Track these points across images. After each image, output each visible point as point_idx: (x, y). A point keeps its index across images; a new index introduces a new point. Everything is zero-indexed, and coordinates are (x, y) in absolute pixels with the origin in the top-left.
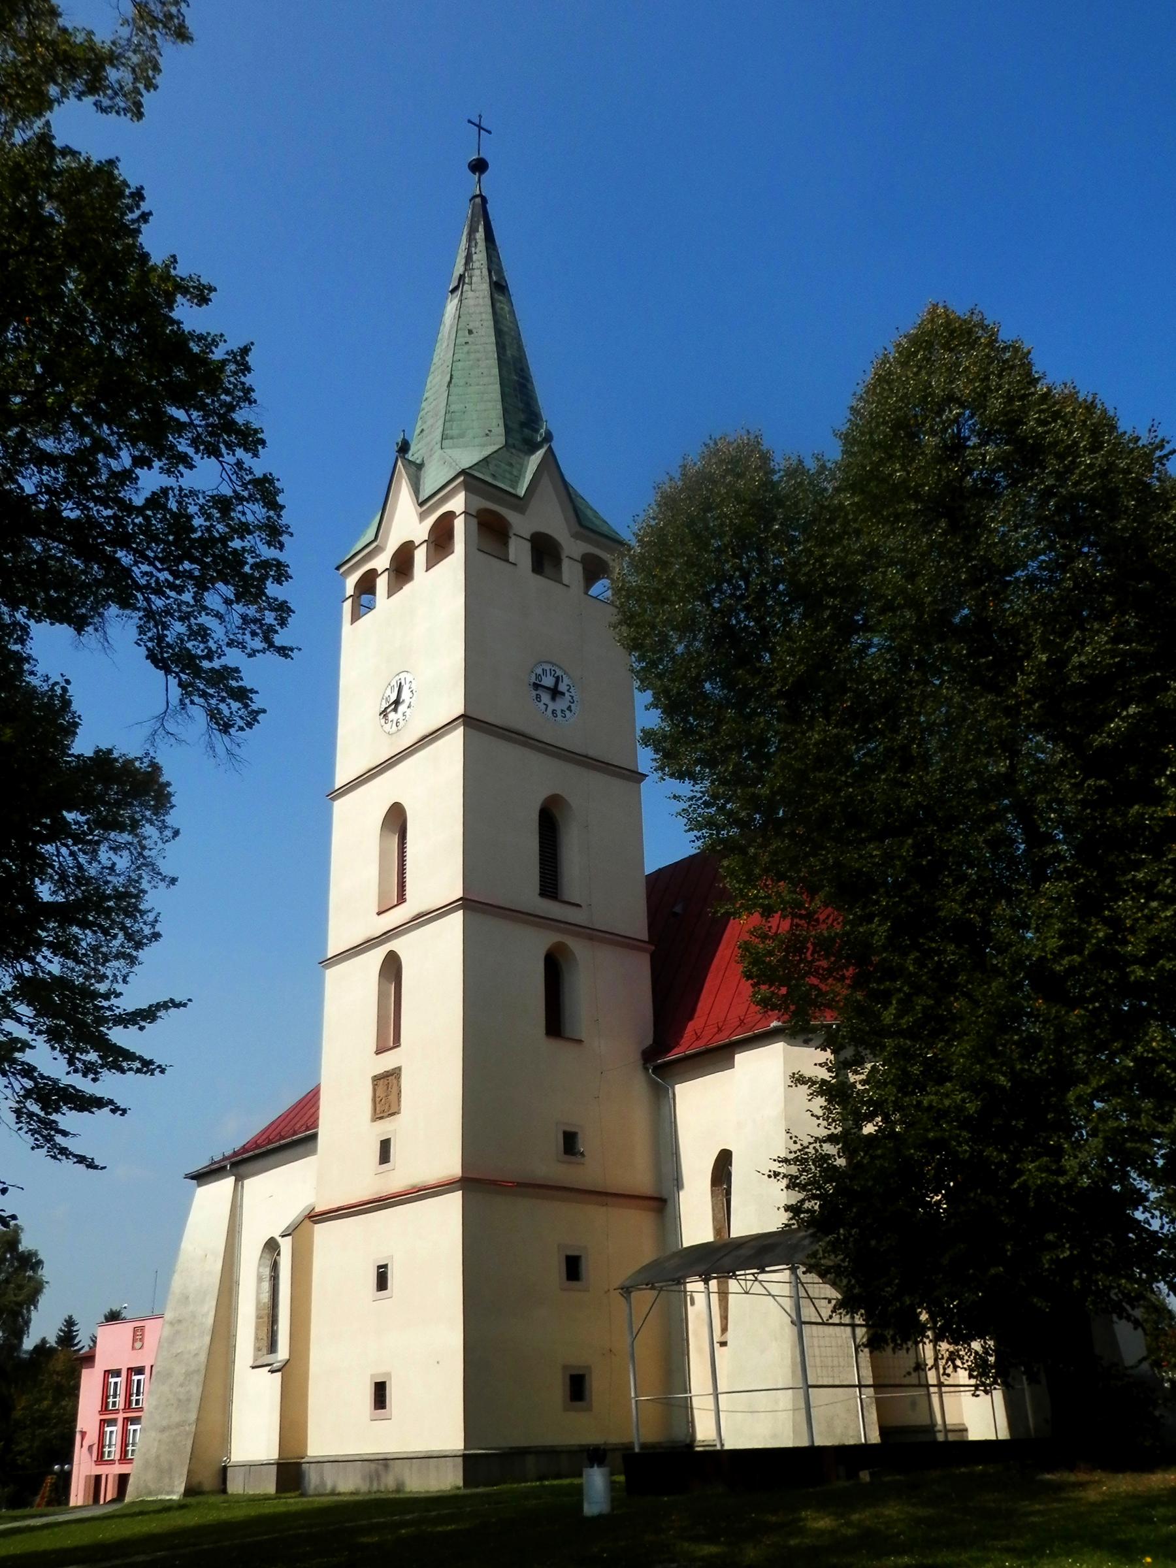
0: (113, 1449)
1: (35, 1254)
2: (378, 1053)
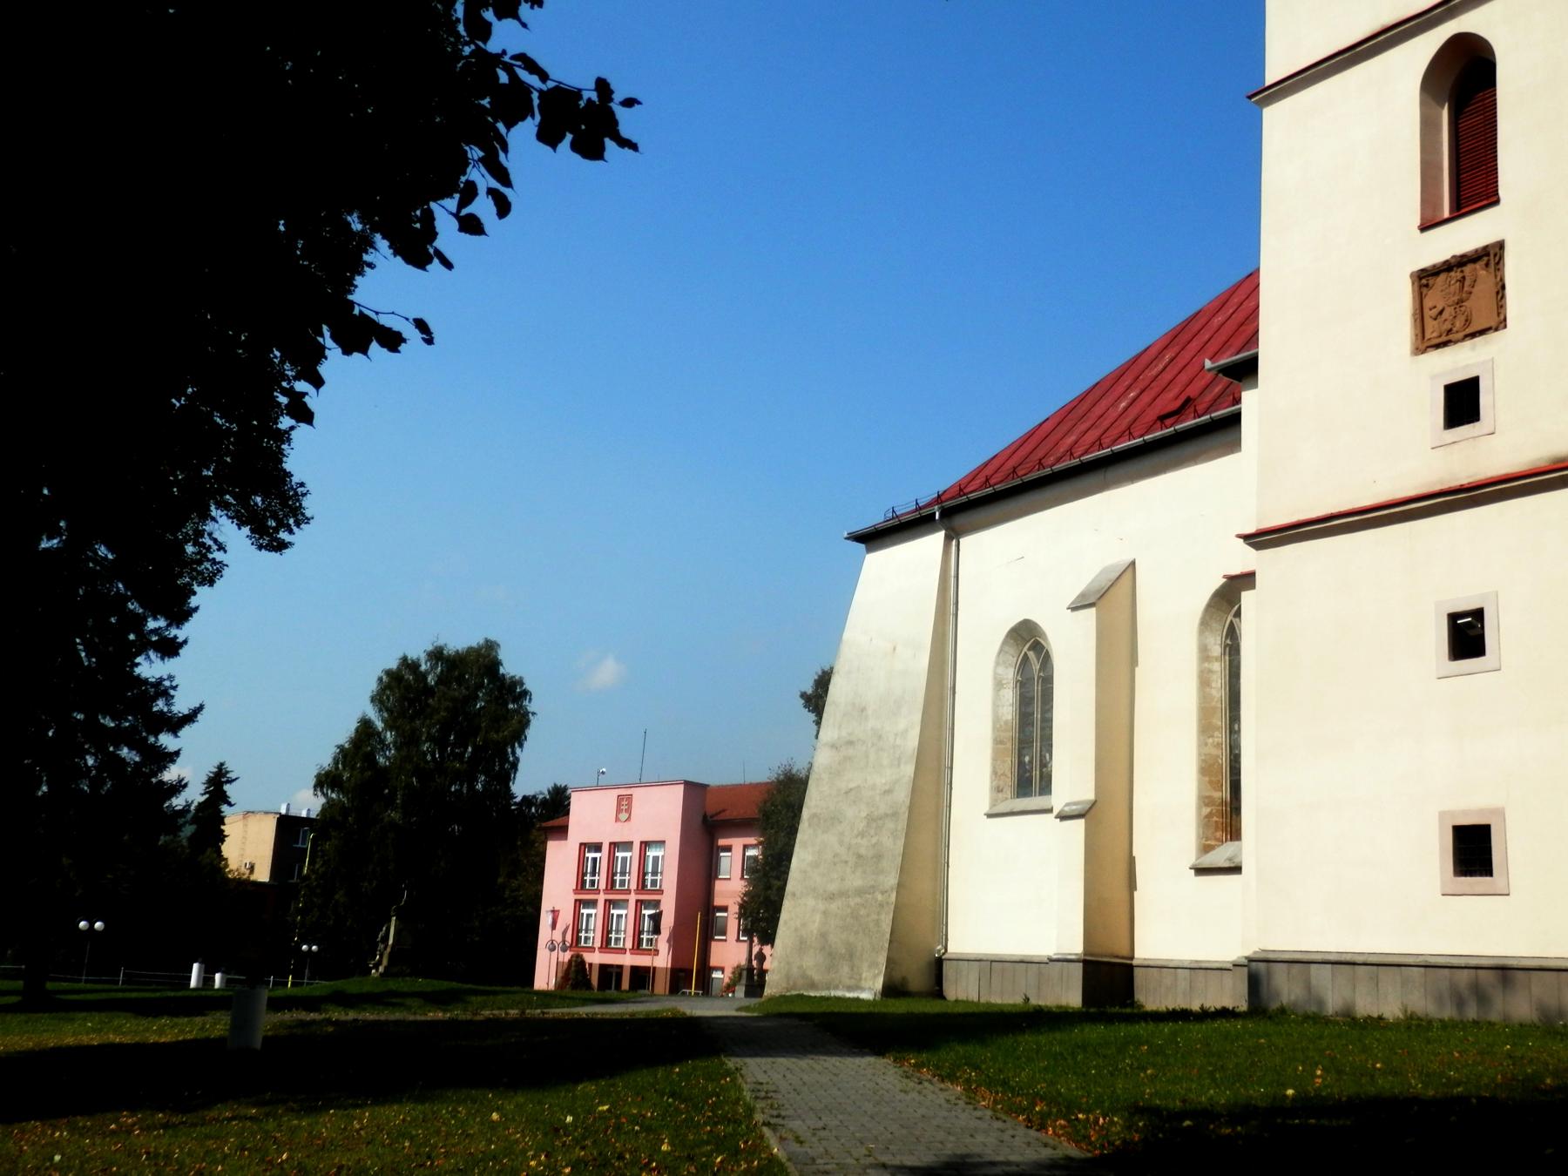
0: (591, 935)
1: (521, 683)
2: (1424, 228)
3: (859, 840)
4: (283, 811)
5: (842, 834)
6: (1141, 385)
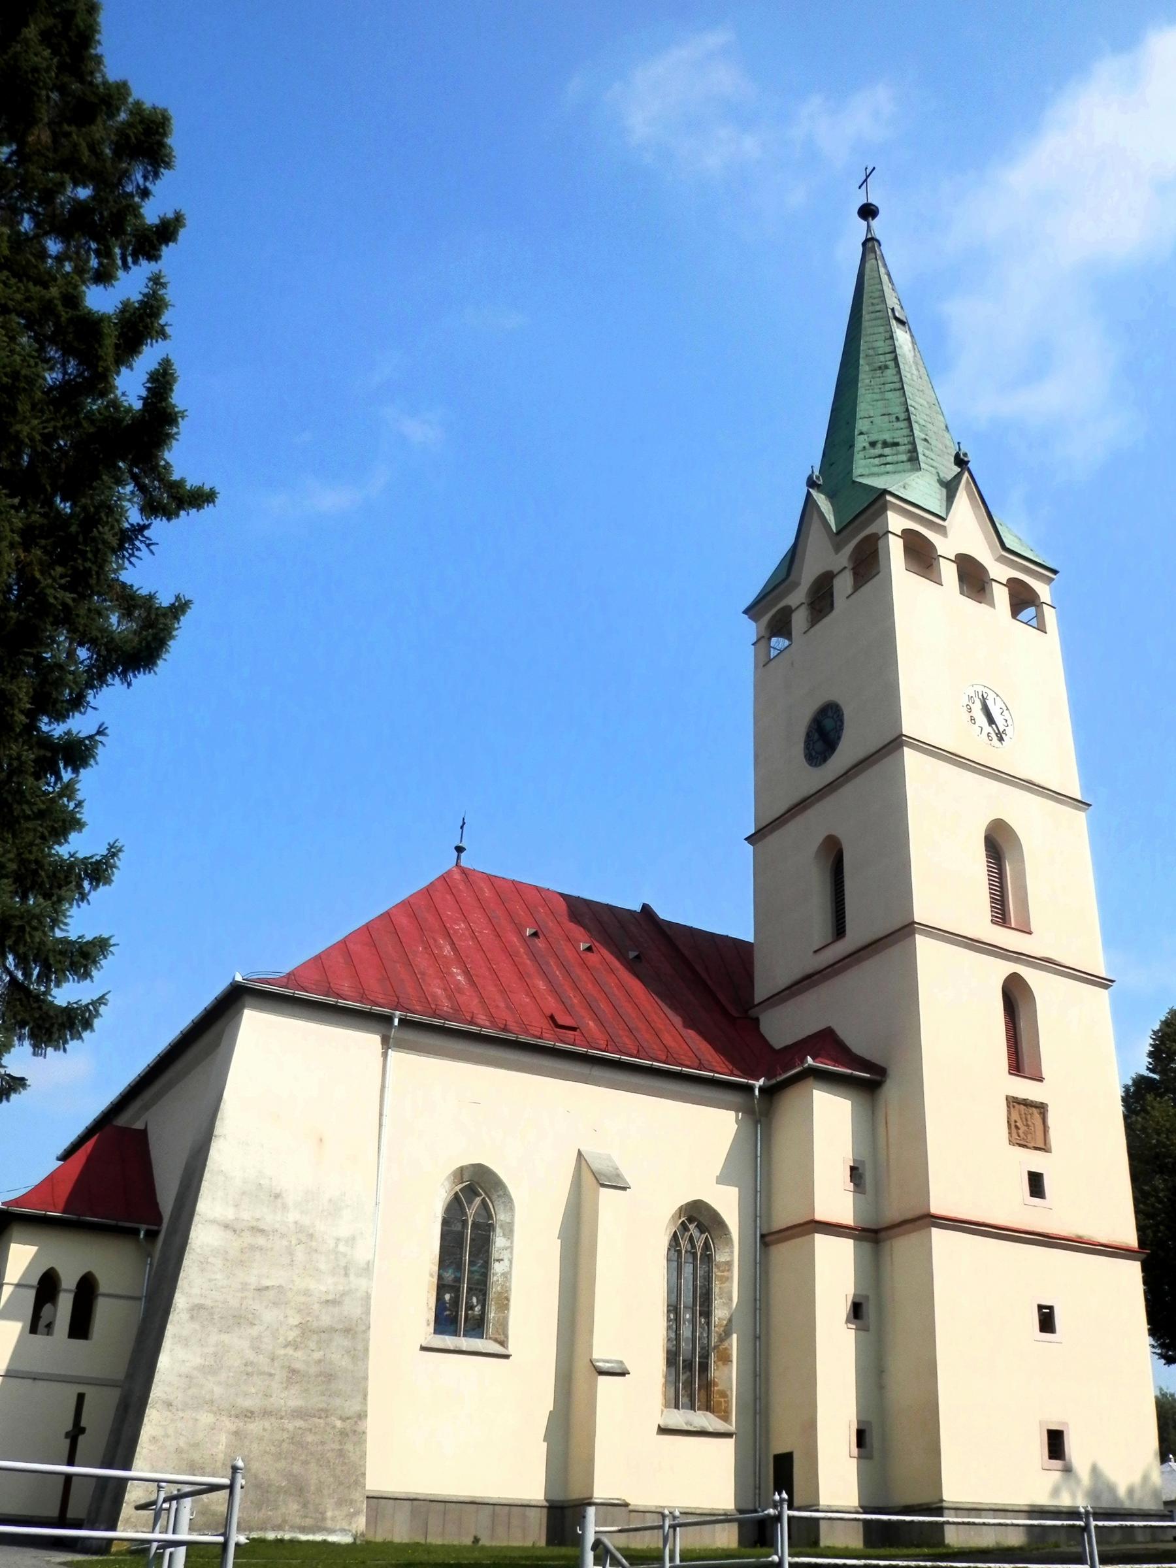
3: (290, 1351)
4: (112, 942)
6: (883, 460)
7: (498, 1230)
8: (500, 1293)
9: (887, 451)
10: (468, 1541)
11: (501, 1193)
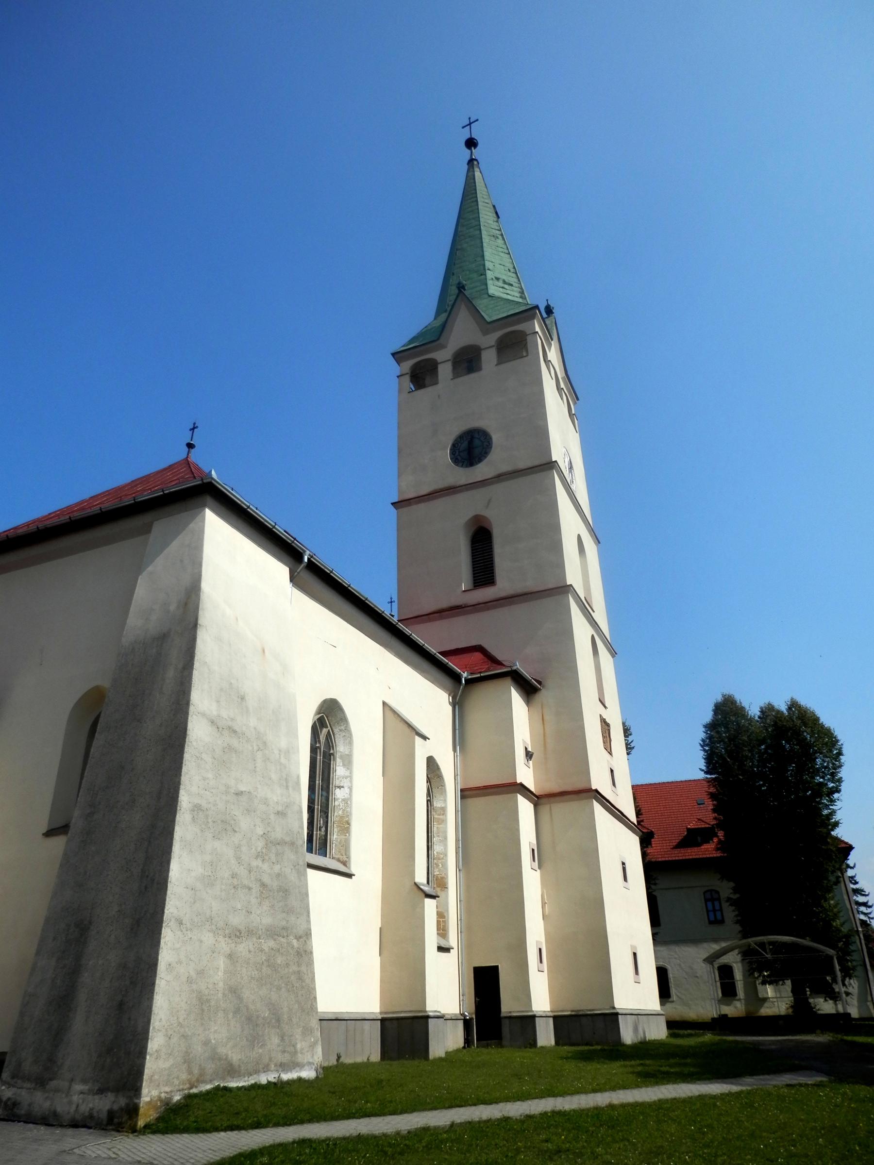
5: (238, 847)
7: (338, 760)
8: (341, 817)
9: (506, 286)
10: (365, 1060)
11: (343, 728)
